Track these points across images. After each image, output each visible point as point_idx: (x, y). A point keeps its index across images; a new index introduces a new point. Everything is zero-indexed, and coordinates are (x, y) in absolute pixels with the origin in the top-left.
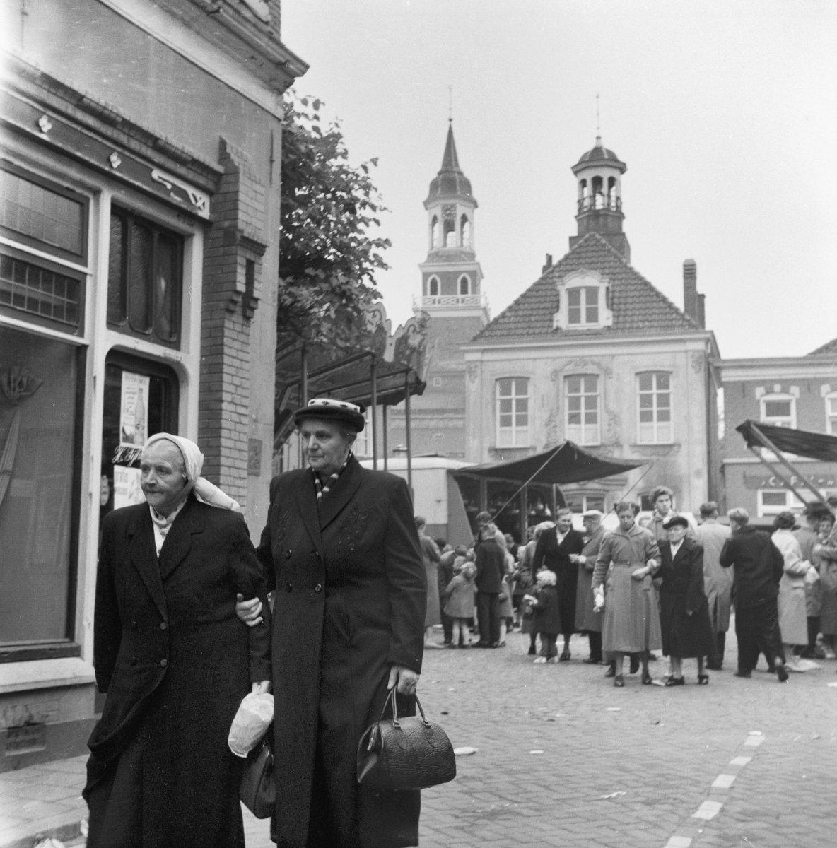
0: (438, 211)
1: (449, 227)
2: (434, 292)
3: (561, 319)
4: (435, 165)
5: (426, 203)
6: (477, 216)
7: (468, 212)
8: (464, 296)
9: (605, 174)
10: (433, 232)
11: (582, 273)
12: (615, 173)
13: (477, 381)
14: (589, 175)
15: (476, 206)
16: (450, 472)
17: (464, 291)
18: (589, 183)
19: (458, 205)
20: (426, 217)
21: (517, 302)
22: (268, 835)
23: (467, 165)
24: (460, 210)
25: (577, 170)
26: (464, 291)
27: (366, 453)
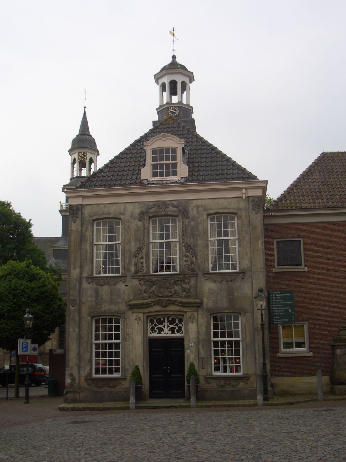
0: (76, 156)
3: (146, 173)
4: (75, 132)
5: (70, 151)
7: (93, 157)
9: (179, 79)
10: (73, 167)
11: (164, 136)
12: (187, 80)
13: (78, 221)
14: (166, 80)
15: (99, 154)
16: (214, 371)
19: (88, 153)
20: (68, 159)
21: (111, 162)
22: (328, 150)
23: (93, 132)
24: (89, 156)
25: (157, 77)
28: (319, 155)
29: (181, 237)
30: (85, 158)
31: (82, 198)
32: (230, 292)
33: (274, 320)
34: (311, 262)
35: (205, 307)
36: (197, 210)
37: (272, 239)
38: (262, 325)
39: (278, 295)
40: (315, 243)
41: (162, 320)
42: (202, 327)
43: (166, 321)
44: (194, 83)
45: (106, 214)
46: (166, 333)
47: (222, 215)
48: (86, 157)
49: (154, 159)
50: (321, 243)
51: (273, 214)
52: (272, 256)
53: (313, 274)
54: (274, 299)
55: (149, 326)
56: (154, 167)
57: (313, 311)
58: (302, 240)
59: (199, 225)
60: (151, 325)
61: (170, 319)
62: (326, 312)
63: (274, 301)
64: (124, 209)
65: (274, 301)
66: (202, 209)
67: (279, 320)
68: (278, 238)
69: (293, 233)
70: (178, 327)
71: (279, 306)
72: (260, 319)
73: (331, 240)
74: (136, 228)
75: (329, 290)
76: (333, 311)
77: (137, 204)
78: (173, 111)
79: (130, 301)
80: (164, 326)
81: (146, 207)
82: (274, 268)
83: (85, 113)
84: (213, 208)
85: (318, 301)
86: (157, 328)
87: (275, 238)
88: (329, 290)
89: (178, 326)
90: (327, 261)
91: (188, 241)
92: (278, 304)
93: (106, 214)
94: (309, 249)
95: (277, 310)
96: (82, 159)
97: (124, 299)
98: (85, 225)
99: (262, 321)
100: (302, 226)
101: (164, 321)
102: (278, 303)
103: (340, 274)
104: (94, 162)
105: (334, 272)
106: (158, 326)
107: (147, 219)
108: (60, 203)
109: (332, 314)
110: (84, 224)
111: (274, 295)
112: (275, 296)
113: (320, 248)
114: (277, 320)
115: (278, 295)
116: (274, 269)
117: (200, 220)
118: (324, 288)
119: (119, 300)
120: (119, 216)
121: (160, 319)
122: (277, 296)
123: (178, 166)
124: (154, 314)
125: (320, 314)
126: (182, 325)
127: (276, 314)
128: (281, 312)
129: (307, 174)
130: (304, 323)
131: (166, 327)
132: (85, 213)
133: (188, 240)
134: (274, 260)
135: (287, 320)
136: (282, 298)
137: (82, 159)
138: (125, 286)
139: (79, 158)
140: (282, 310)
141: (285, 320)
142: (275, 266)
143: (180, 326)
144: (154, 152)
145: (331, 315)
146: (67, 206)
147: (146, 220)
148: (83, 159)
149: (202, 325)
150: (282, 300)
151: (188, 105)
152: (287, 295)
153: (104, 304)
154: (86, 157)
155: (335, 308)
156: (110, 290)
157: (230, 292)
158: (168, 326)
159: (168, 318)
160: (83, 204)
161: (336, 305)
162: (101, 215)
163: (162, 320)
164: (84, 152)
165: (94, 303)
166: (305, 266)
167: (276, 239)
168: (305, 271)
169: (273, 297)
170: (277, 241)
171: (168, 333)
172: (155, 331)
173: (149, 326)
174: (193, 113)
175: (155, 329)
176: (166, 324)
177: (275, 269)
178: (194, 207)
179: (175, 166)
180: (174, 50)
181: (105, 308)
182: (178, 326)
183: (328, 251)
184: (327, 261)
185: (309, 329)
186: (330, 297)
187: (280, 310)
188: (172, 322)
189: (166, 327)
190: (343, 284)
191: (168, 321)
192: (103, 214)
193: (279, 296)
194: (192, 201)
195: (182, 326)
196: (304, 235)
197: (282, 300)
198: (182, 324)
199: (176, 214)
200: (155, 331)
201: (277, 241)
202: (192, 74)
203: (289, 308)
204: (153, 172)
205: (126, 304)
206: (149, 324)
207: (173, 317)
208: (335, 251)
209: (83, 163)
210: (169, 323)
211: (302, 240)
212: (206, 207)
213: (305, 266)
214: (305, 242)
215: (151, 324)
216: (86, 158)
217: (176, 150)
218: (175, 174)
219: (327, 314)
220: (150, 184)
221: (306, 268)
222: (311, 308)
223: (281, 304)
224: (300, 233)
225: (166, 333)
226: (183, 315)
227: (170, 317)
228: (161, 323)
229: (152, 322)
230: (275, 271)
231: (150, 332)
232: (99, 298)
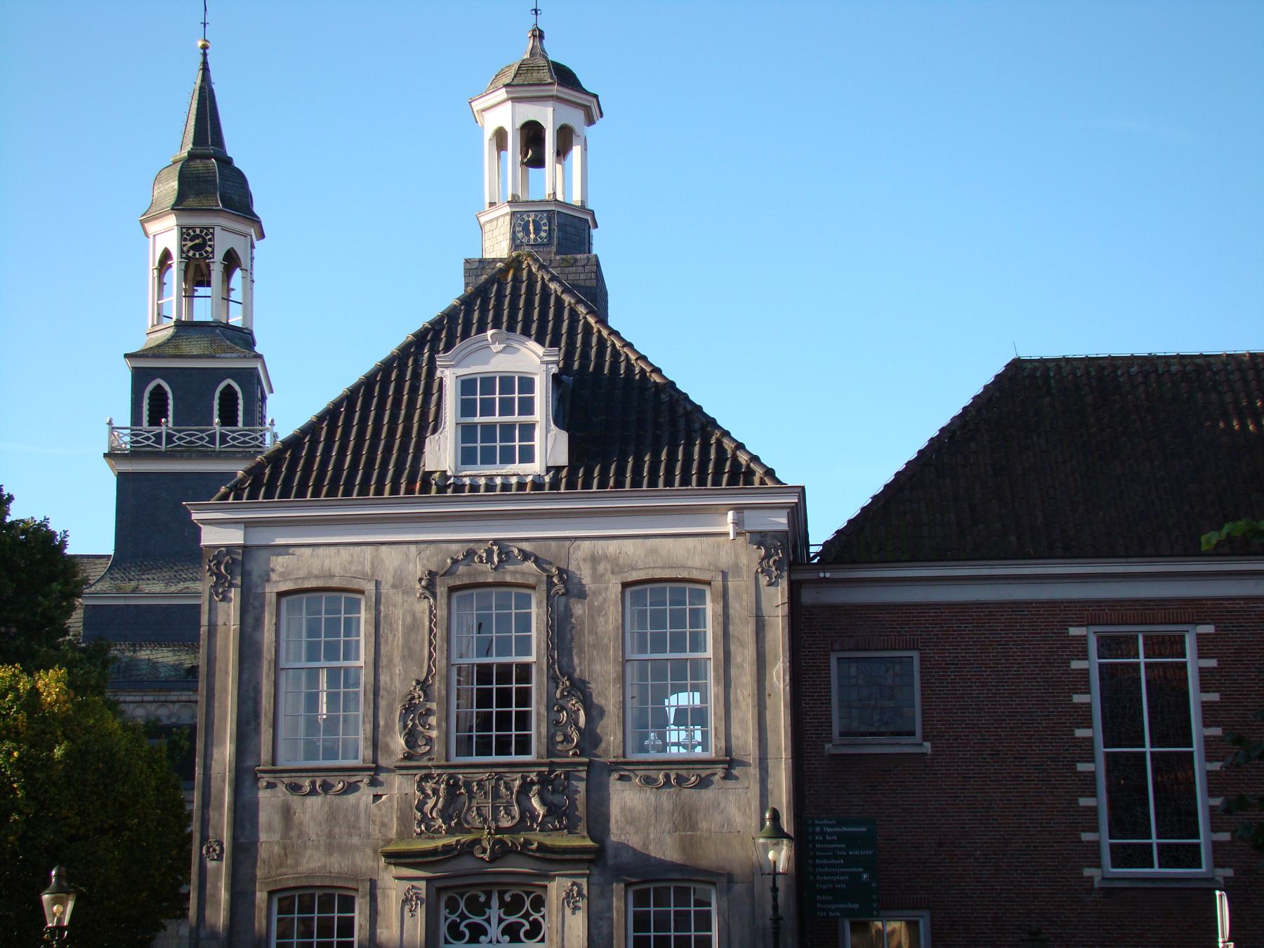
1: (196, 275)
2: (157, 414)
6: (264, 255)
7: (239, 245)
8: (225, 430)
12: (575, 118)
15: (262, 235)
17: (228, 418)
18: (513, 141)
19: (217, 230)
24: (222, 243)
26: (228, 418)
27: (447, 760)
28: (999, 368)
29: (544, 651)
30: (209, 249)
31: (245, 527)
32: (686, 820)
33: (819, 905)
34: (941, 725)
35: (611, 862)
36: (594, 569)
37: (824, 651)
38: (776, 919)
39: (829, 830)
40: (956, 668)
41: (482, 899)
42: (601, 923)
43: (495, 902)
44: (600, 122)
45: (317, 577)
46: (494, 939)
47: (668, 585)
48: (210, 246)
49: (467, 408)
50: (977, 668)
51: (828, 575)
52: (823, 704)
53: (949, 762)
54: (819, 842)
55: (442, 919)
56: (467, 432)
57: (946, 878)
58: (915, 655)
59: (599, 616)
60: (448, 916)
61: (507, 898)
62: (986, 882)
63: (818, 846)
64: (372, 562)
65: (818, 846)
66: (609, 567)
67: (834, 907)
68: (843, 650)
69: (890, 636)
70: (530, 922)
71: (833, 861)
72: (770, 900)
73: (1006, 660)
74: (409, 619)
75: (998, 816)
76: (1010, 882)
77: (413, 548)
78: (532, 231)
79: (389, 842)
80: (489, 918)
81: (439, 557)
82: (830, 742)
83: (205, 68)
84: (641, 565)
85: (963, 847)
86: (465, 926)
87: (835, 648)
88: (998, 816)
89: (531, 919)
90: (993, 724)
91: (564, 663)
92: (828, 858)
93: (317, 577)
94: (936, 687)
95: (828, 874)
96: (197, 256)
97: (368, 835)
98: (254, 608)
99: (775, 907)
100: (919, 613)
101: (487, 904)
102: (831, 854)
103: (1033, 765)
104: (243, 267)
105: (1015, 758)
106: (470, 918)
107: (441, 595)
108: (110, 423)
109: (1005, 889)
110: (251, 607)
111: (818, 829)
112: (823, 833)
113: (973, 683)
114: (828, 906)
115: (829, 830)
116: (828, 746)
117: (601, 599)
118: (982, 808)
119: (355, 840)
120: (356, 584)
121: (477, 897)
122: (826, 833)
123: (538, 433)
124: (459, 882)
125: (969, 890)
126: (543, 917)
127: (825, 887)
128: (839, 882)
129: (951, 438)
130: (920, 916)
131: (494, 921)
132: (252, 571)
133: (566, 659)
134: (831, 718)
135: (856, 906)
136: (842, 837)
137: (197, 256)
138: (374, 796)
139: (182, 251)
140: (842, 874)
141: (850, 905)
142: (831, 738)
143: (535, 920)
144: (467, 386)
145: (1000, 893)
146: (135, 439)
147: (438, 597)
148: (201, 254)
149: (601, 919)
150: (843, 846)
151: (583, 208)
152: (857, 830)
153: (308, 852)
154: (210, 246)
155: (1016, 870)
156: (327, 808)
157: (686, 820)
158: (501, 920)
159: (501, 894)
160: (249, 543)
161: (1018, 862)
162: (303, 578)
163: (482, 899)
164: (202, 229)
165: (276, 849)
166: (925, 738)
167: (837, 651)
168: (926, 754)
169: (814, 833)
170: (838, 658)
171: (500, 939)
172: (462, 936)
173: (442, 919)
174: (596, 226)
175: (462, 928)
176: (495, 912)
177: (830, 745)
178: (585, 560)
179: (527, 431)
180: (536, 11)
181: (312, 865)
182: (531, 919)
183: (996, 693)
184: (993, 724)
185: (932, 933)
186: (1000, 835)
187: (835, 874)
188: (512, 907)
189: (494, 921)
190: (1041, 796)
191: (502, 904)
192: (309, 576)
193: (832, 834)
194: (578, 543)
195: (485, 924)
196: (925, 642)
197: (843, 846)
198: (542, 914)
199: (531, 581)
200: (462, 936)
201: (838, 658)
202: (595, 100)
203: (861, 870)
204: (462, 400)
205: (375, 851)
206: (444, 912)
207: (516, 891)
208: (1020, 693)
209: (198, 267)
210: (502, 911)
211: (915, 655)
212: (621, 560)
213: (925, 738)
214: (926, 665)
215: (449, 913)
216: (213, 252)
217: (532, 381)
218: (527, 456)
219: (989, 889)
220: (448, 487)
221: (927, 744)
222: (941, 870)
223: (836, 857)
224: (910, 635)
225: (494, 939)
226: (546, 887)
227: (506, 891)
228: (478, 908)
229: (452, 906)
230: (833, 752)
231: (445, 937)
232: (294, 834)
